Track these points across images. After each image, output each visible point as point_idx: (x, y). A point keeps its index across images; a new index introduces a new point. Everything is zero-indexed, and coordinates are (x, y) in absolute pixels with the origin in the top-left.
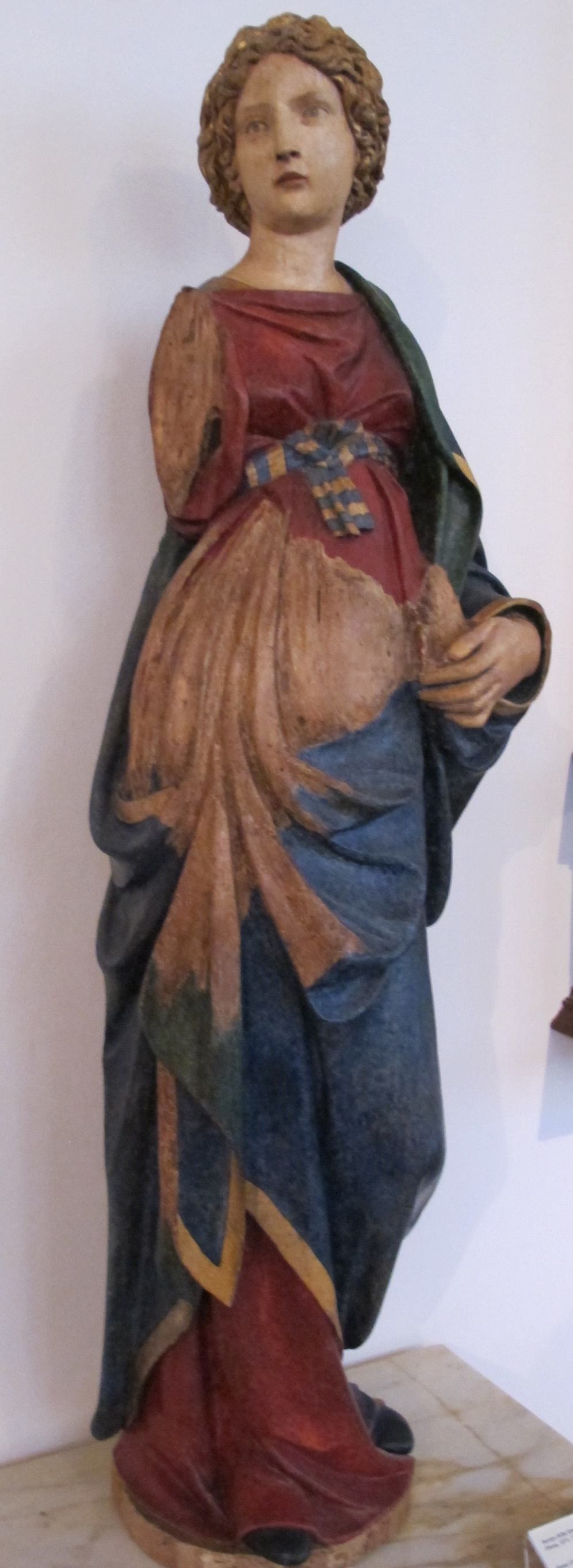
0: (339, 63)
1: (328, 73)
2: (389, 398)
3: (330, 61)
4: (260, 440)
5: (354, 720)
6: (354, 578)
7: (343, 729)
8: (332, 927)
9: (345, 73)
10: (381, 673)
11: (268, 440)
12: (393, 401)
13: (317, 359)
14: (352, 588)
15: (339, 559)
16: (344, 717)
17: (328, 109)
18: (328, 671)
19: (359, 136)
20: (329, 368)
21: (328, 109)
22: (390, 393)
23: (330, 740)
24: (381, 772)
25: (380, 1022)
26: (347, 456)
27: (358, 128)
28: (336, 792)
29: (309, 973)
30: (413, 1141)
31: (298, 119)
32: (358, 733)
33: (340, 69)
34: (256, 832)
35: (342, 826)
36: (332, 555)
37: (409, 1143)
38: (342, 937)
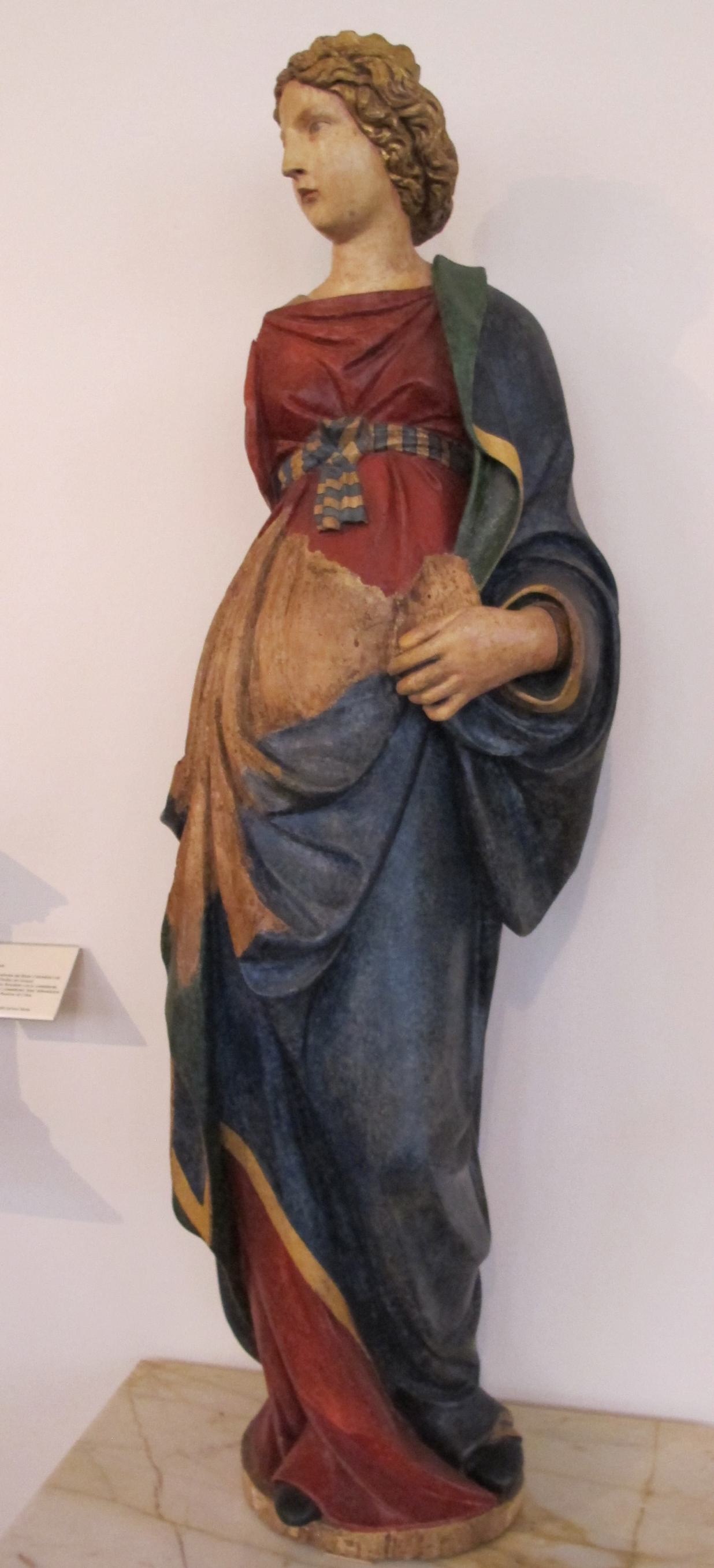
0: (332, 74)
1: (324, 86)
2: (403, 389)
3: (319, 74)
4: (283, 445)
5: (310, 708)
6: (325, 570)
7: (298, 716)
8: (252, 903)
9: (339, 81)
10: (340, 663)
11: (292, 443)
12: (409, 390)
13: (327, 362)
14: (319, 580)
15: (318, 552)
16: (299, 706)
17: (329, 120)
18: (287, 660)
19: (373, 136)
20: (337, 368)
21: (329, 120)
22: (410, 380)
23: (287, 727)
24: (328, 759)
25: (346, 1010)
26: (352, 451)
27: (370, 129)
28: (268, 774)
29: (241, 944)
30: (374, 1137)
31: (305, 136)
32: (313, 720)
33: (332, 79)
34: (221, 808)
35: (277, 809)
36: (312, 548)
37: (369, 1138)
38: (259, 914)
